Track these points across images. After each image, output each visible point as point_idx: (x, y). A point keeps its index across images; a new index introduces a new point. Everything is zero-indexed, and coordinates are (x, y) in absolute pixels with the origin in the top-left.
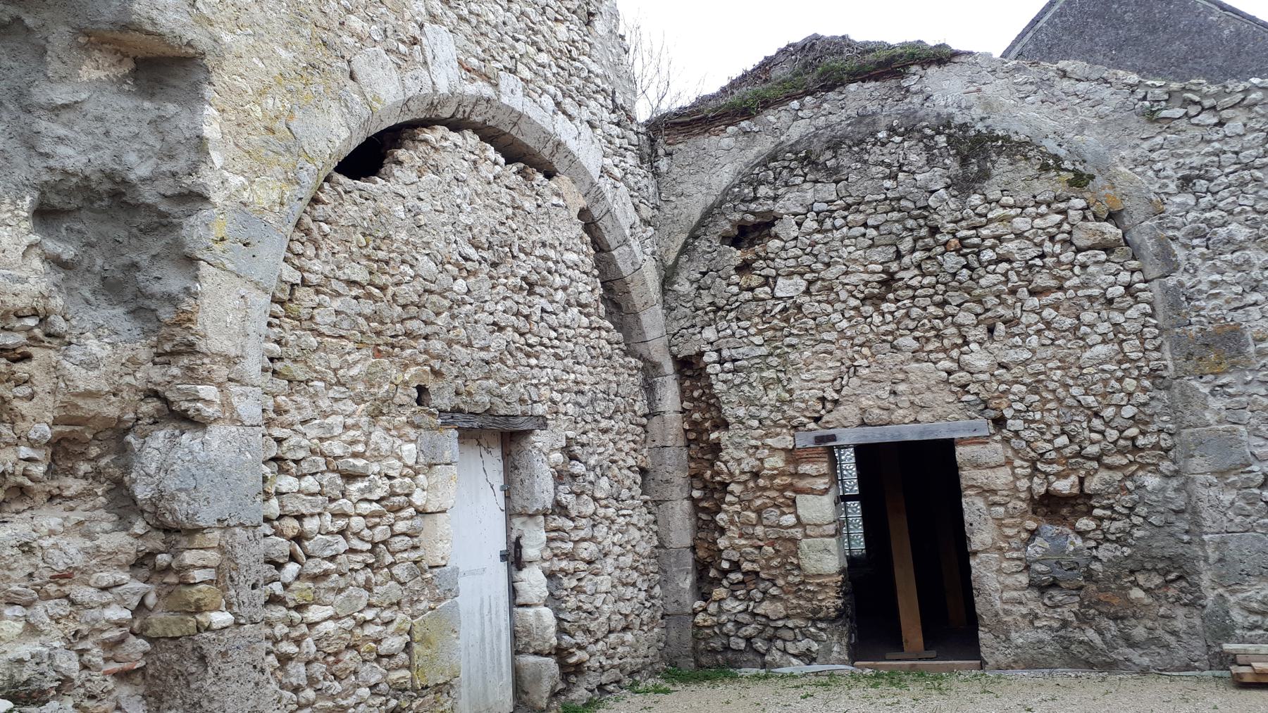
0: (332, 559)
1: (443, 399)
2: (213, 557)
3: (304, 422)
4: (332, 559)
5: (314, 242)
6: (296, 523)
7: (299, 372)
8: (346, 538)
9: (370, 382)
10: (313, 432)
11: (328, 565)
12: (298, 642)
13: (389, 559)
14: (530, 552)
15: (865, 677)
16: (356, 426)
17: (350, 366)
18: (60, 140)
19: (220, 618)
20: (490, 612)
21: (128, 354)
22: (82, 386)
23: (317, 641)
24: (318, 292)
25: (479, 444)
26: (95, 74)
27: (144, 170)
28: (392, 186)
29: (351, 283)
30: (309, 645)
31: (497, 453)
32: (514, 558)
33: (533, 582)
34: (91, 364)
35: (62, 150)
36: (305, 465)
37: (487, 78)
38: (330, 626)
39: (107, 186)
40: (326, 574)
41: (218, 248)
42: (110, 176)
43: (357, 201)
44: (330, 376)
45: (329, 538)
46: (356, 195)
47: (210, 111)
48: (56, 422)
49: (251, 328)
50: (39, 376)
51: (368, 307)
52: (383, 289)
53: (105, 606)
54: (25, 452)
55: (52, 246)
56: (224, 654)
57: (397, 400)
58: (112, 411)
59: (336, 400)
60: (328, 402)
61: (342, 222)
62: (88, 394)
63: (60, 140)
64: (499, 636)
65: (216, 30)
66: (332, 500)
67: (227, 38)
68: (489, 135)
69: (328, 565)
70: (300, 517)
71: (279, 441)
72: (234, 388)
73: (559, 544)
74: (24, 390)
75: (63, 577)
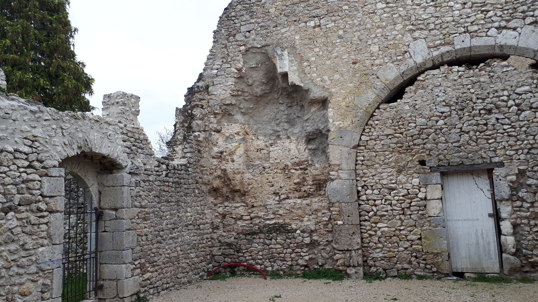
0: (387, 211)
1: (432, 162)
2: (337, 209)
3: (373, 176)
4: (387, 211)
5: (373, 127)
6: (373, 202)
7: (369, 163)
8: (391, 206)
9: (397, 161)
10: (376, 178)
11: (385, 213)
12: (375, 231)
13: (409, 213)
14: (503, 215)
15: (354, 266)
16: (392, 175)
17: (389, 159)
18: (308, 126)
19: (340, 222)
20: (482, 234)
21: (323, 166)
22: (314, 174)
23: (382, 232)
24: (376, 141)
25: (472, 174)
26: (314, 109)
27: (322, 127)
28: (403, 100)
29: (387, 135)
30: (379, 233)
31: (487, 177)
32: (497, 217)
33: (506, 226)
34: (317, 169)
35: (308, 128)
36: (374, 187)
37: (448, 44)
38: (386, 229)
39: (318, 132)
40: (384, 215)
41: (332, 141)
42: (317, 130)
43: (388, 111)
44: (381, 162)
45: (384, 206)
46: (388, 109)
47: (330, 110)
48: (313, 181)
49: (343, 157)
50: (309, 173)
51: (395, 140)
52: (402, 133)
53: (323, 217)
54: (309, 187)
55: (310, 147)
56: (340, 230)
57: (408, 166)
58: (323, 178)
59: (384, 169)
60: (381, 170)
61: (383, 118)
62: (318, 175)
63: (308, 126)
64: (489, 243)
65: (330, 90)
66: (384, 196)
67: (333, 90)
68: (458, 62)
69: (385, 213)
70: (375, 200)
71: (365, 181)
72: (339, 171)
73: (519, 213)
74: (307, 175)
75: (316, 210)
